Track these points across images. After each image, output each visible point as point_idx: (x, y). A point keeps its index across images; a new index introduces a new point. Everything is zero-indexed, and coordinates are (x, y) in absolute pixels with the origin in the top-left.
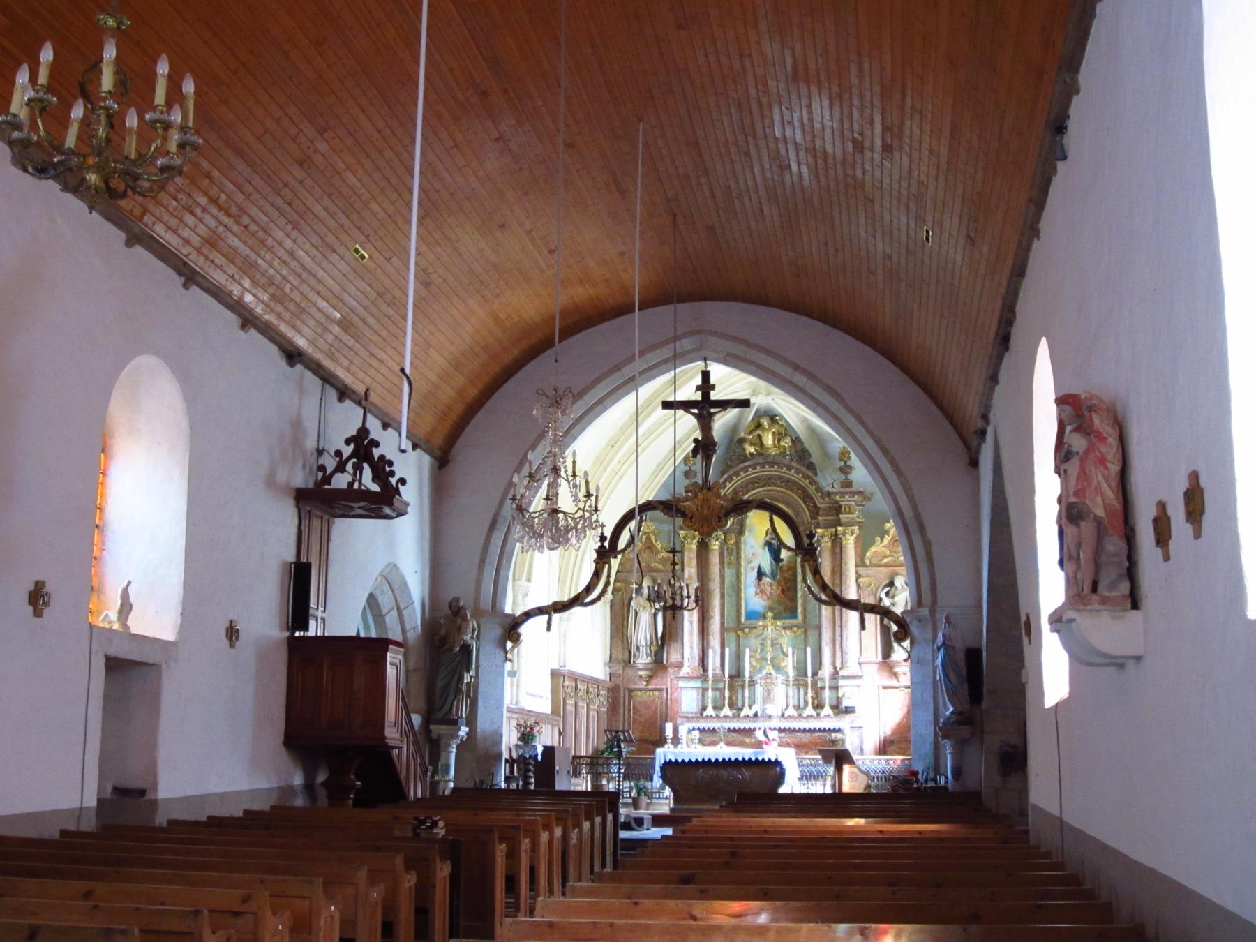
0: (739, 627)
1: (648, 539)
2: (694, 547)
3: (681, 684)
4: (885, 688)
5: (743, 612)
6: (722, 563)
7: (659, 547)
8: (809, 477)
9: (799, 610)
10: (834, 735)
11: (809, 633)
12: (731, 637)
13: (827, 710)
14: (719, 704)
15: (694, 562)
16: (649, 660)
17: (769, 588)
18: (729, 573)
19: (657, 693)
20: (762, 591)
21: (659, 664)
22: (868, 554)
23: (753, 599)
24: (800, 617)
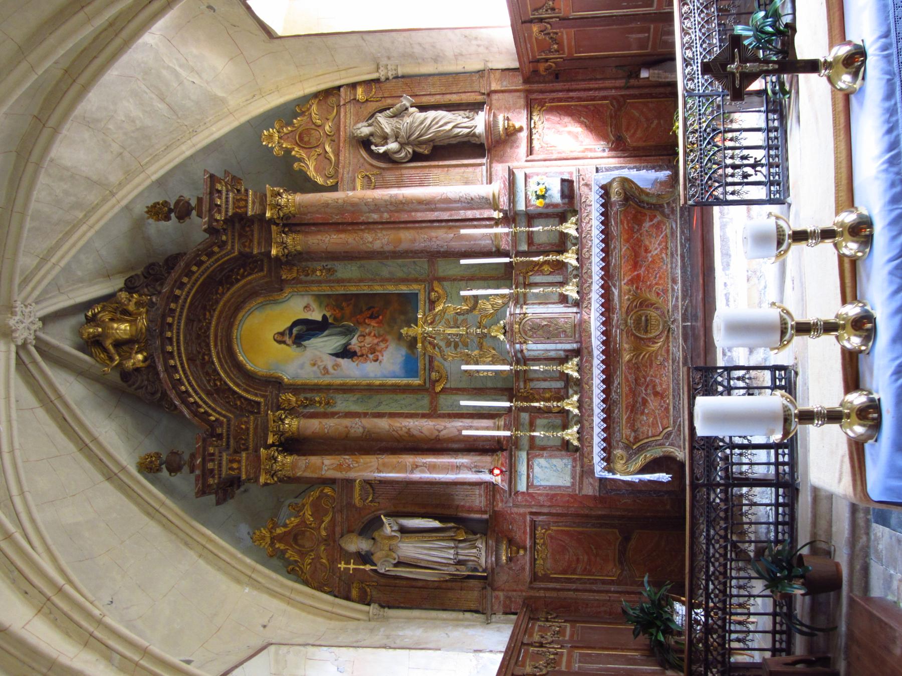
0: (427, 389)
1: (281, 538)
2: (289, 459)
3: (522, 486)
4: (531, 151)
5: (405, 381)
6: (325, 415)
7: (294, 521)
8: (188, 265)
9: (404, 289)
10: (614, 198)
11: (441, 274)
12: (445, 402)
13: (569, 228)
14: (558, 421)
15: (315, 460)
16: (480, 544)
17: (368, 339)
18: (343, 404)
19: (540, 531)
20: (373, 350)
21: (490, 526)
22: (320, 180)
23: (386, 365)
24: (415, 287)
